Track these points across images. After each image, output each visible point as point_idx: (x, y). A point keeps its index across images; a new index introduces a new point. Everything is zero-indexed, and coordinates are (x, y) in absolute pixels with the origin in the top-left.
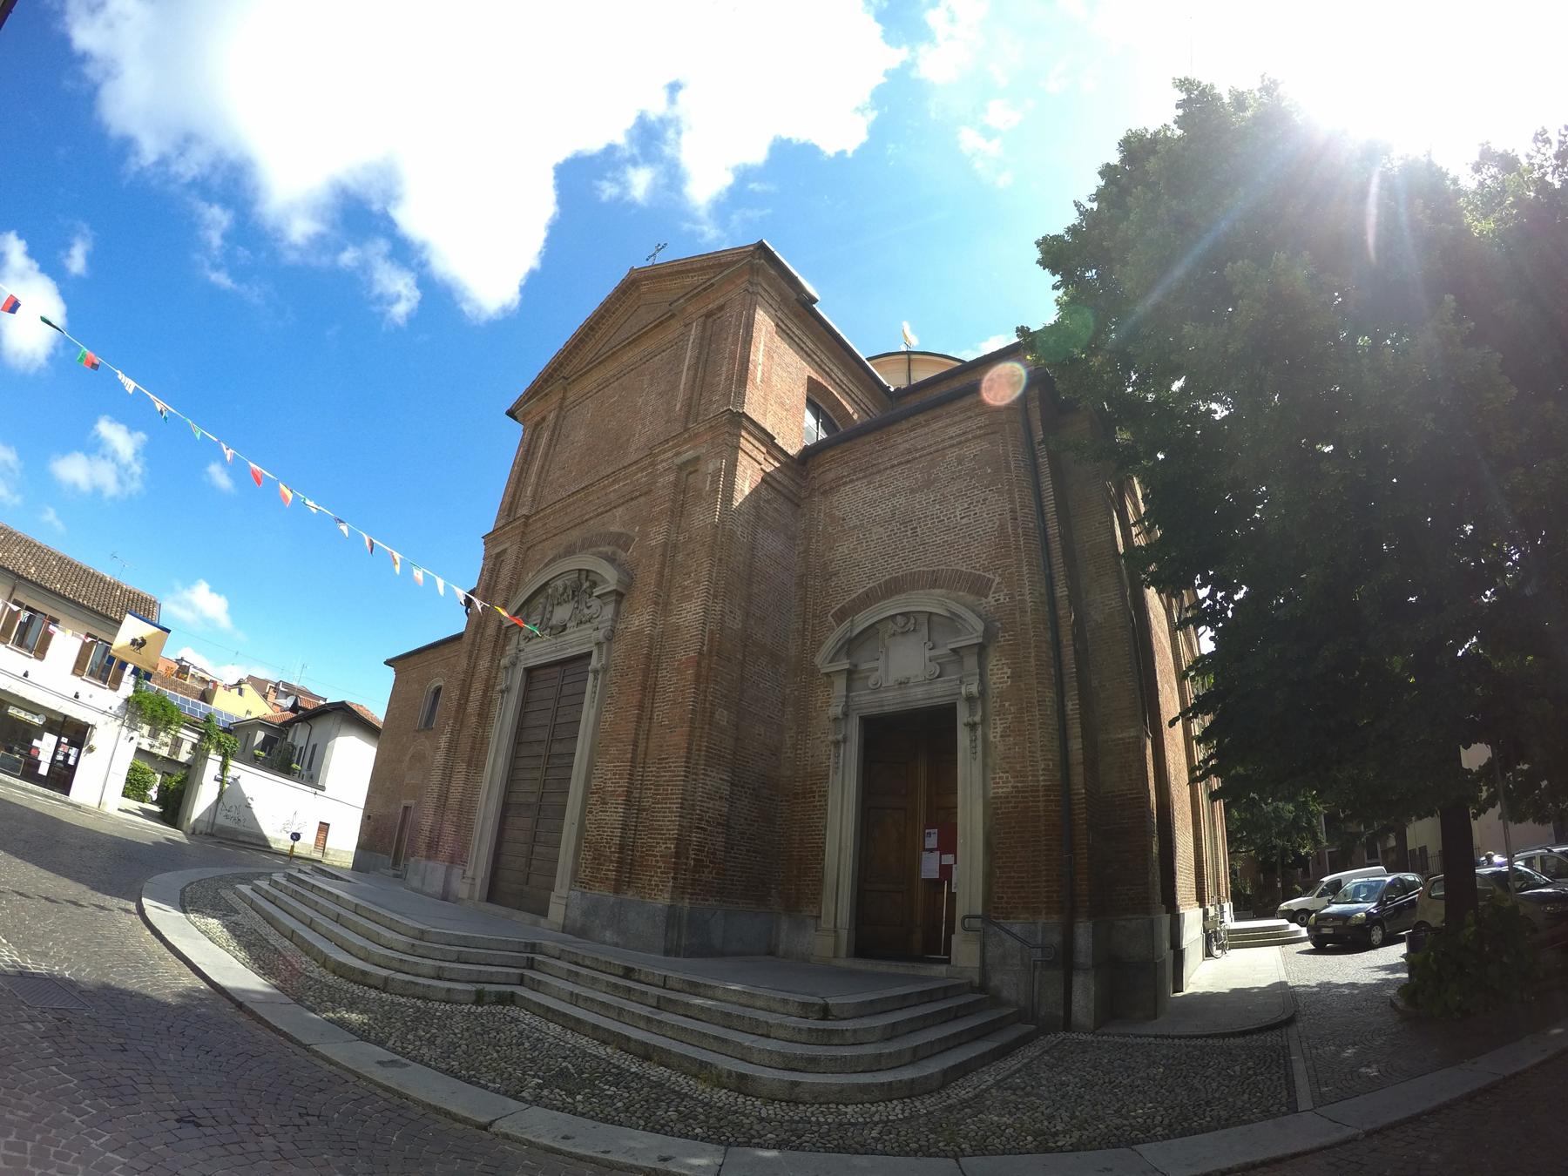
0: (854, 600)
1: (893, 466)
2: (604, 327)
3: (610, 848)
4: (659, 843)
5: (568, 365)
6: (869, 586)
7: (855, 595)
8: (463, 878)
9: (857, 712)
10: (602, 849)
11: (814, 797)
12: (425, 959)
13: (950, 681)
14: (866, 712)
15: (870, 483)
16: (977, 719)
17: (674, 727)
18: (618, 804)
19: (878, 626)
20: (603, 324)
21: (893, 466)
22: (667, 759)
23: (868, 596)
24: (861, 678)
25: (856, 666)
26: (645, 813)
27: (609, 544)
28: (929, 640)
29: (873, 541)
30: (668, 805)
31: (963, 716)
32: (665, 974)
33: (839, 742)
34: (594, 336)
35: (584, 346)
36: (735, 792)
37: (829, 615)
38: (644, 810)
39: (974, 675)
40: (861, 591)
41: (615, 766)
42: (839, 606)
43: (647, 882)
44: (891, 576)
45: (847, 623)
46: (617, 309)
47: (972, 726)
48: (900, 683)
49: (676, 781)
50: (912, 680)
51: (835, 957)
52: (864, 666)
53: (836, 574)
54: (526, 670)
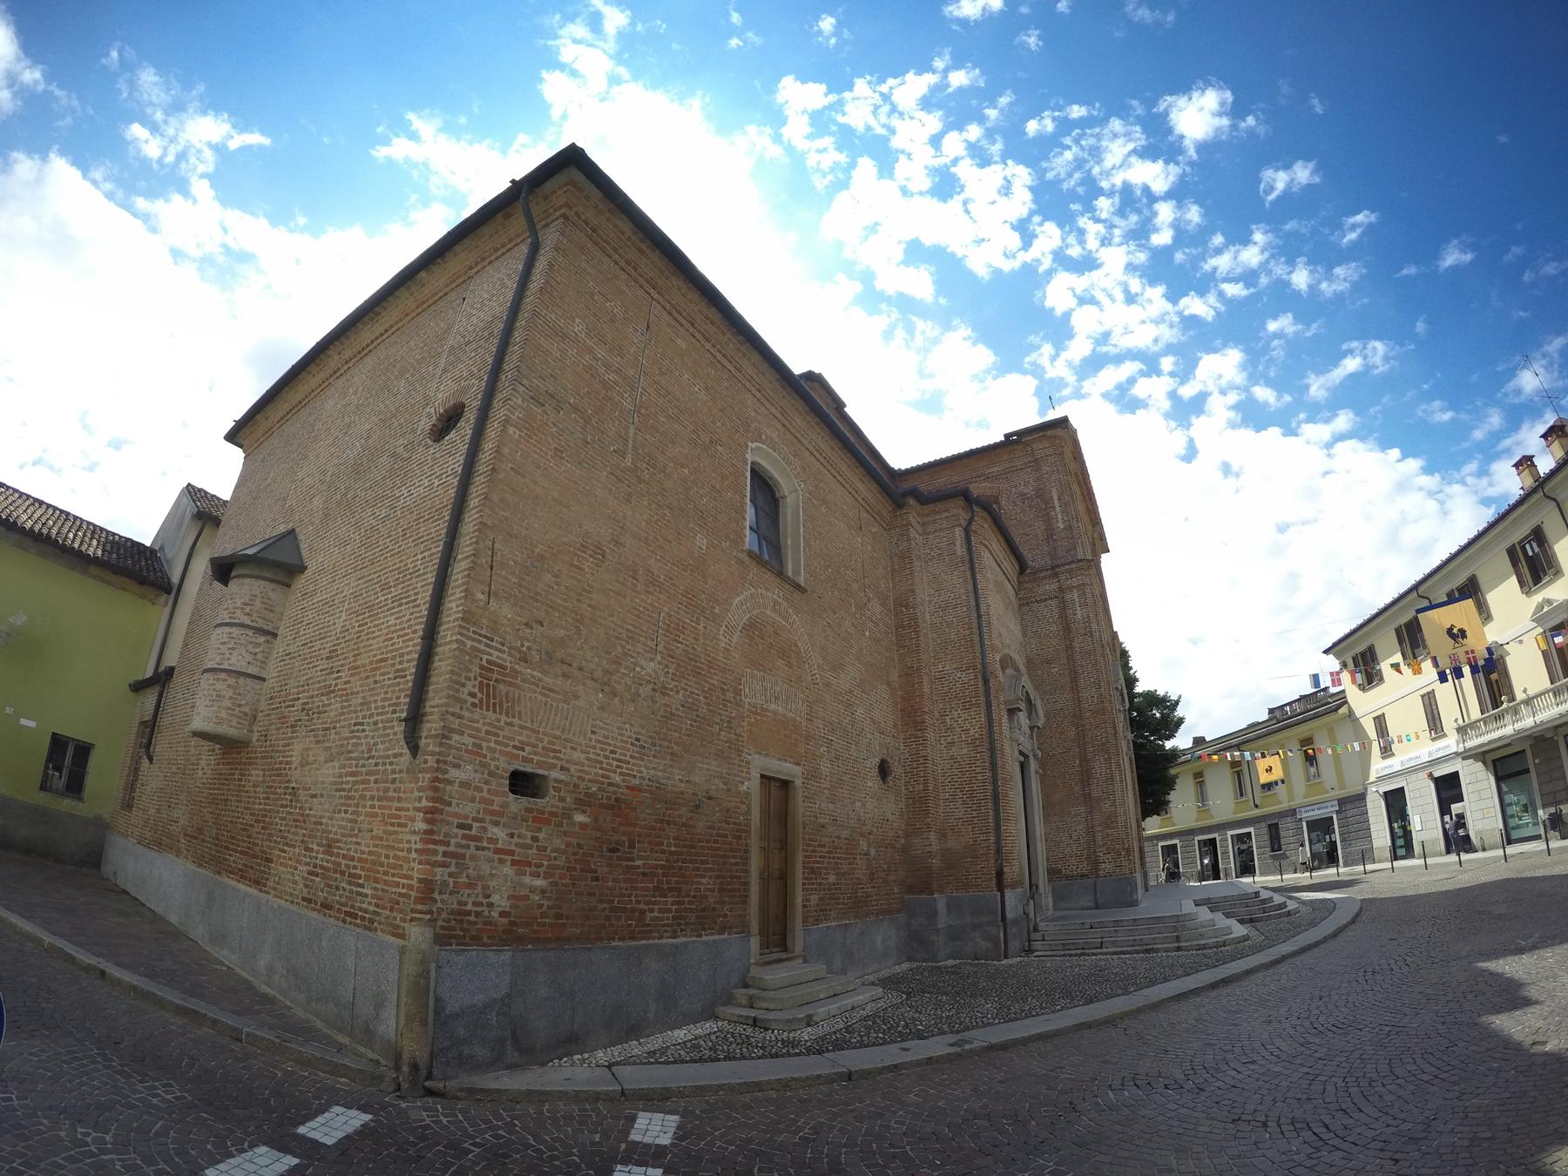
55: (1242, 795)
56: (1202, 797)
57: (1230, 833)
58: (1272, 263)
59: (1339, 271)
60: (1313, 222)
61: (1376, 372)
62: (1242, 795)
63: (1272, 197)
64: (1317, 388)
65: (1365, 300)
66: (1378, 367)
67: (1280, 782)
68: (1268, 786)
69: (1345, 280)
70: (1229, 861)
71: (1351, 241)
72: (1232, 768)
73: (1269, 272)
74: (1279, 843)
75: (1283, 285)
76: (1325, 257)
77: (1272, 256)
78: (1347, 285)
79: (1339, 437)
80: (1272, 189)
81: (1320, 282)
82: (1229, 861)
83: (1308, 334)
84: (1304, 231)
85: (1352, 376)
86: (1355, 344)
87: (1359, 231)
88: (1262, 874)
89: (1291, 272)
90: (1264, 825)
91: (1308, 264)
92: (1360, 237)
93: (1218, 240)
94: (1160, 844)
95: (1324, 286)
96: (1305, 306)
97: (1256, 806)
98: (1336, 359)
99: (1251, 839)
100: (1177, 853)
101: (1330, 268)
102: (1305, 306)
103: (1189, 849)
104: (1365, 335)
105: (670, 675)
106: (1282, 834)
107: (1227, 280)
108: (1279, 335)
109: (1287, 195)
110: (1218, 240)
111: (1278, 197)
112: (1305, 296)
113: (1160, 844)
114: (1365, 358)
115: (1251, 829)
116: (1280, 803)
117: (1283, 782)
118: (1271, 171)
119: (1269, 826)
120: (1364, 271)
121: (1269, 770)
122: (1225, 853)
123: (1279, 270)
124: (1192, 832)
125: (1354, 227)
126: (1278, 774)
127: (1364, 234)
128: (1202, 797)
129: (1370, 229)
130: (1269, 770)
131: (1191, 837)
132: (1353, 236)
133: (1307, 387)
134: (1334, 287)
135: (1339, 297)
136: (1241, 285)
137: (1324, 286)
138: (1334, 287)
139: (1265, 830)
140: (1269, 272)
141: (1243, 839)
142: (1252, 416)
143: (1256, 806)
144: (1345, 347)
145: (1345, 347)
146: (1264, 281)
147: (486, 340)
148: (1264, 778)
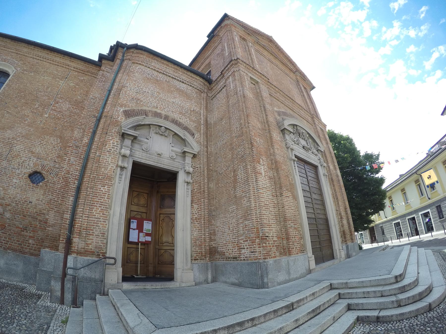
55: (422, 195)
56: (406, 199)
57: (420, 213)
58: (402, 30)
59: (423, 28)
60: (410, 15)
61: (444, 56)
62: (422, 195)
63: (395, 11)
64: (428, 65)
65: (433, 34)
66: (443, 54)
67: (436, 183)
68: (432, 186)
69: (425, 30)
70: (421, 227)
71: (423, 17)
72: (416, 183)
73: (402, 34)
74: (442, 214)
75: (408, 37)
76: (417, 24)
77: (402, 29)
78: (426, 31)
79: (439, 80)
80: (394, 9)
81: (418, 33)
82: (421, 227)
83: (420, 50)
84: (408, 18)
85: (437, 59)
86: (434, 49)
87: (424, 13)
88: (437, 230)
89: (408, 32)
90: (434, 207)
91: (413, 28)
92: (425, 15)
93: (384, 29)
94: (393, 223)
95: (420, 34)
96: (417, 42)
97: (429, 199)
98: (430, 55)
99: (430, 214)
100: (400, 226)
101: (420, 27)
102: (417, 42)
103: (405, 223)
104: (437, 45)
106: (443, 210)
107: (391, 41)
108: (411, 53)
109: (400, 10)
110: (384, 29)
111: (397, 11)
112: (415, 38)
113: (393, 223)
114: (439, 52)
115: (429, 210)
116: (440, 195)
117: (437, 182)
118: (392, 3)
119: (437, 207)
120: (430, 25)
121: (429, 177)
122: (419, 223)
123: (405, 32)
124: (404, 216)
125: (422, 13)
126: (434, 179)
127: (426, 13)
128: (406, 199)
129: (427, 11)
130: (429, 177)
131: (404, 218)
132: (423, 15)
133: (424, 66)
134: (423, 33)
135: (425, 35)
136: (395, 40)
137: (420, 34)
138: (423, 33)
139: (435, 209)
140: (402, 34)
141: (426, 215)
142: (412, 80)
143: (429, 199)
144: (431, 51)
145: (431, 51)
146: (402, 37)
147: (424, 321)
148: (428, 182)
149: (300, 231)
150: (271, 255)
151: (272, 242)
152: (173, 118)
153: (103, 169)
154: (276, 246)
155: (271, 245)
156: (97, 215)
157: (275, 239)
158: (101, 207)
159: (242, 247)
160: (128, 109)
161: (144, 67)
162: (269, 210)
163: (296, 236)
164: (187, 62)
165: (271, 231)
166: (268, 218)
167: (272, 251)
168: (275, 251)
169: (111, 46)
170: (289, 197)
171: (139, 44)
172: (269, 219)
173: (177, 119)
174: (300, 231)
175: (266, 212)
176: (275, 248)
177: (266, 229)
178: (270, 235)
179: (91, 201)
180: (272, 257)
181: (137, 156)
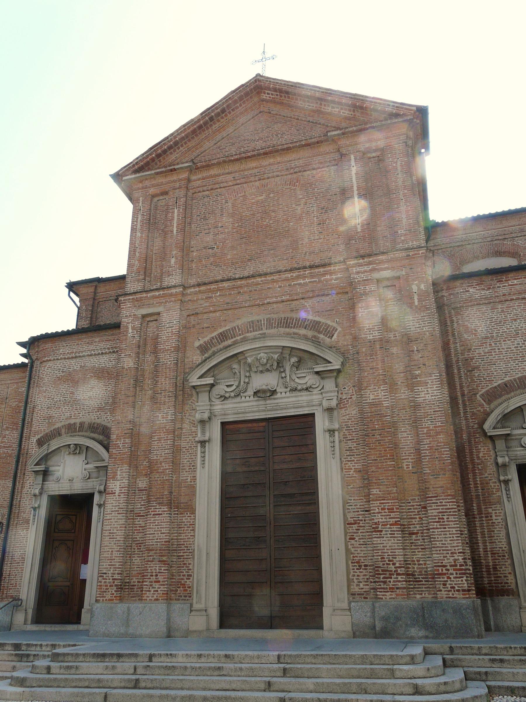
0: (495, 387)
1: (512, 300)
2: (222, 120)
3: (394, 564)
4: (446, 557)
5: (182, 146)
6: (506, 379)
7: (496, 384)
8: (191, 611)
9: (514, 461)
10: (385, 566)
11: (491, 516)
12: (227, 692)
13: (93, 481)
14: (520, 462)
15: (493, 309)
16: (36, 506)
17: (437, 475)
18: (394, 531)
19: (61, 448)
20: (222, 118)
21: (512, 300)
22: (437, 497)
23: (507, 386)
24: (513, 439)
25: (48, 468)
26: (414, 536)
27: (305, 328)
28: (86, 459)
29: (504, 349)
30: (447, 529)
31: (96, 499)
32: (149, 652)
33: (36, 508)
34: (211, 125)
35: (200, 133)
36: (192, 532)
37: (478, 396)
38: (413, 534)
39: (39, 484)
40: (500, 382)
41: (380, 503)
42: (484, 390)
43: (442, 586)
44: (521, 375)
45: (45, 447)
46: (237, 108)
47: (100, 506)
48: (70, 480)
49: (450, 512)
50: (75, 479)
51: (25, 624)
52: (51, 469)
53: (478, 368)
54: (223, 424)
105: (154, 574)
149: (190, 564)
150: (105, 597)
151: (111, 580)
152: (89, 421)
153: (22, 514)
154: (116, 585)
155: (109, 585)
156: (191, 521)
157: (116, 576)
158: (357, 551)
159: (458, 572)
160: (41, 435)
161: (52, 362)
162: (115, 540)
163: (160, 572)
164: (71, 325)
165: (112, 567)
166: (110, 550)
167: (109, 592)
168: (113, 592)
169: (426, 147)
170: (161, 514)
171: (35, 335)
172: (112, 551)
173: (94, 421)
174: (190, 564)
175: (110, 543)
176: (115, 588)
177: (105, 564)
178: (109, 572)
179: (132, 527)
180: (106, 600)
181: (50, 490)
